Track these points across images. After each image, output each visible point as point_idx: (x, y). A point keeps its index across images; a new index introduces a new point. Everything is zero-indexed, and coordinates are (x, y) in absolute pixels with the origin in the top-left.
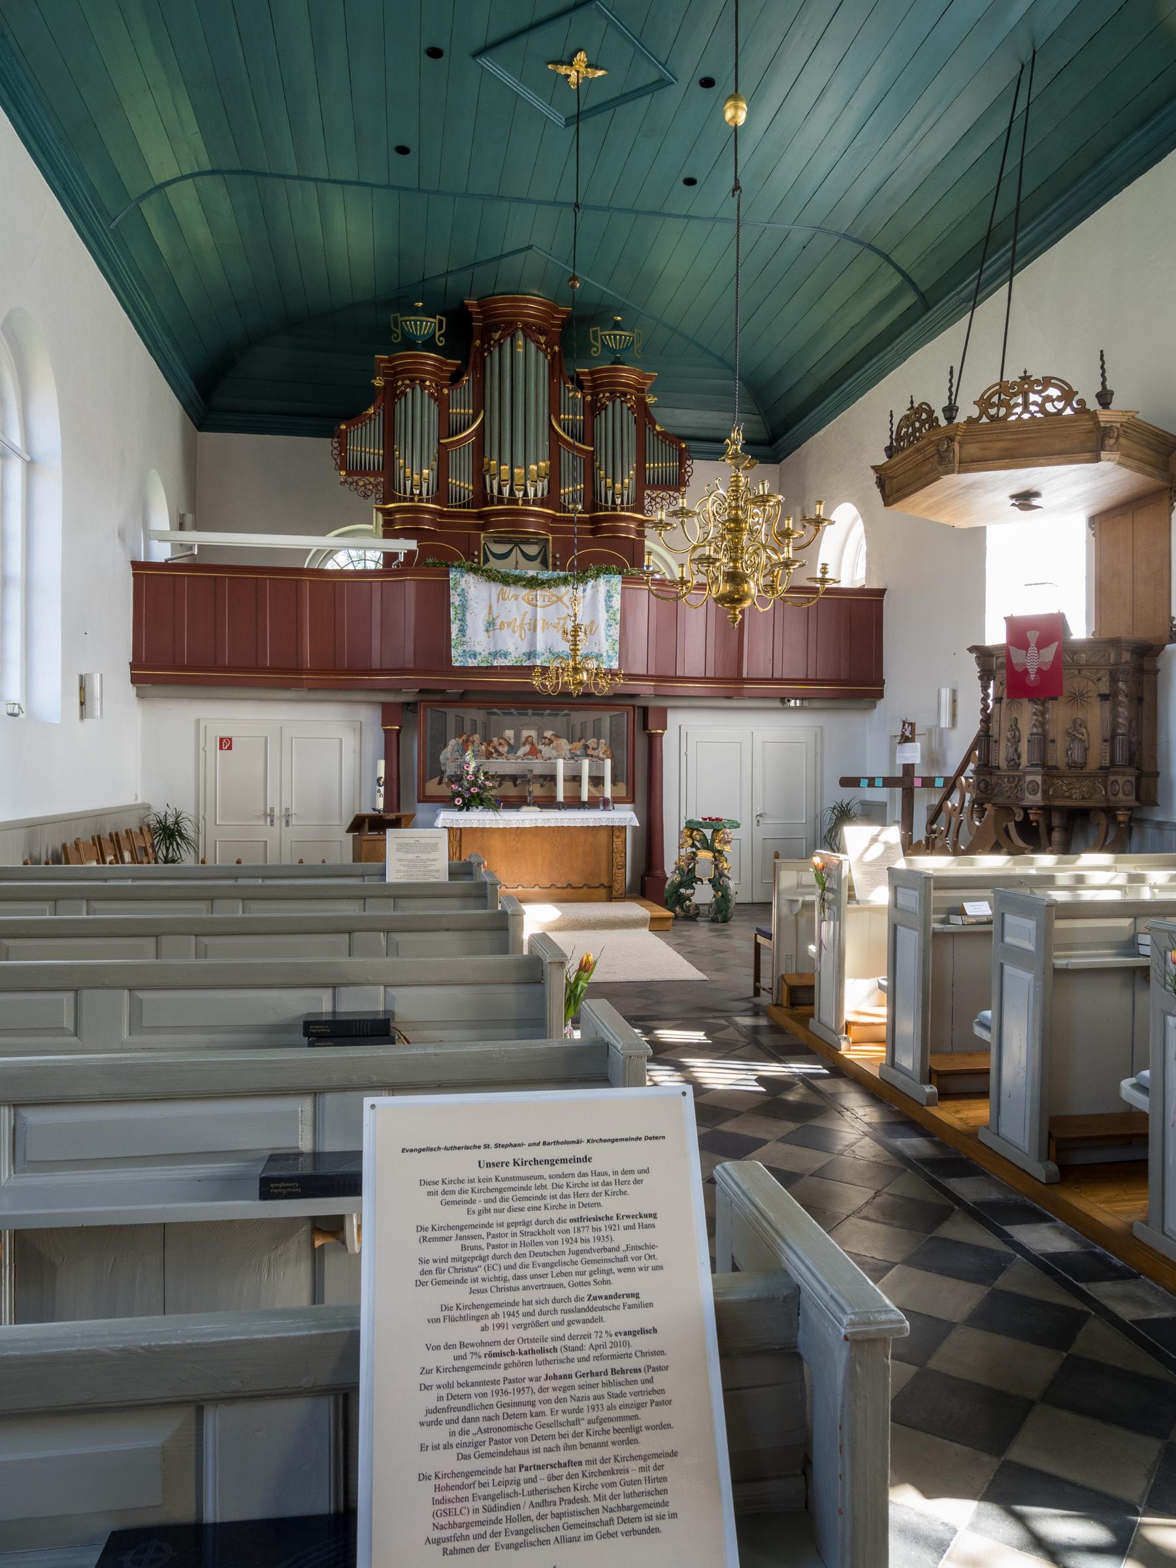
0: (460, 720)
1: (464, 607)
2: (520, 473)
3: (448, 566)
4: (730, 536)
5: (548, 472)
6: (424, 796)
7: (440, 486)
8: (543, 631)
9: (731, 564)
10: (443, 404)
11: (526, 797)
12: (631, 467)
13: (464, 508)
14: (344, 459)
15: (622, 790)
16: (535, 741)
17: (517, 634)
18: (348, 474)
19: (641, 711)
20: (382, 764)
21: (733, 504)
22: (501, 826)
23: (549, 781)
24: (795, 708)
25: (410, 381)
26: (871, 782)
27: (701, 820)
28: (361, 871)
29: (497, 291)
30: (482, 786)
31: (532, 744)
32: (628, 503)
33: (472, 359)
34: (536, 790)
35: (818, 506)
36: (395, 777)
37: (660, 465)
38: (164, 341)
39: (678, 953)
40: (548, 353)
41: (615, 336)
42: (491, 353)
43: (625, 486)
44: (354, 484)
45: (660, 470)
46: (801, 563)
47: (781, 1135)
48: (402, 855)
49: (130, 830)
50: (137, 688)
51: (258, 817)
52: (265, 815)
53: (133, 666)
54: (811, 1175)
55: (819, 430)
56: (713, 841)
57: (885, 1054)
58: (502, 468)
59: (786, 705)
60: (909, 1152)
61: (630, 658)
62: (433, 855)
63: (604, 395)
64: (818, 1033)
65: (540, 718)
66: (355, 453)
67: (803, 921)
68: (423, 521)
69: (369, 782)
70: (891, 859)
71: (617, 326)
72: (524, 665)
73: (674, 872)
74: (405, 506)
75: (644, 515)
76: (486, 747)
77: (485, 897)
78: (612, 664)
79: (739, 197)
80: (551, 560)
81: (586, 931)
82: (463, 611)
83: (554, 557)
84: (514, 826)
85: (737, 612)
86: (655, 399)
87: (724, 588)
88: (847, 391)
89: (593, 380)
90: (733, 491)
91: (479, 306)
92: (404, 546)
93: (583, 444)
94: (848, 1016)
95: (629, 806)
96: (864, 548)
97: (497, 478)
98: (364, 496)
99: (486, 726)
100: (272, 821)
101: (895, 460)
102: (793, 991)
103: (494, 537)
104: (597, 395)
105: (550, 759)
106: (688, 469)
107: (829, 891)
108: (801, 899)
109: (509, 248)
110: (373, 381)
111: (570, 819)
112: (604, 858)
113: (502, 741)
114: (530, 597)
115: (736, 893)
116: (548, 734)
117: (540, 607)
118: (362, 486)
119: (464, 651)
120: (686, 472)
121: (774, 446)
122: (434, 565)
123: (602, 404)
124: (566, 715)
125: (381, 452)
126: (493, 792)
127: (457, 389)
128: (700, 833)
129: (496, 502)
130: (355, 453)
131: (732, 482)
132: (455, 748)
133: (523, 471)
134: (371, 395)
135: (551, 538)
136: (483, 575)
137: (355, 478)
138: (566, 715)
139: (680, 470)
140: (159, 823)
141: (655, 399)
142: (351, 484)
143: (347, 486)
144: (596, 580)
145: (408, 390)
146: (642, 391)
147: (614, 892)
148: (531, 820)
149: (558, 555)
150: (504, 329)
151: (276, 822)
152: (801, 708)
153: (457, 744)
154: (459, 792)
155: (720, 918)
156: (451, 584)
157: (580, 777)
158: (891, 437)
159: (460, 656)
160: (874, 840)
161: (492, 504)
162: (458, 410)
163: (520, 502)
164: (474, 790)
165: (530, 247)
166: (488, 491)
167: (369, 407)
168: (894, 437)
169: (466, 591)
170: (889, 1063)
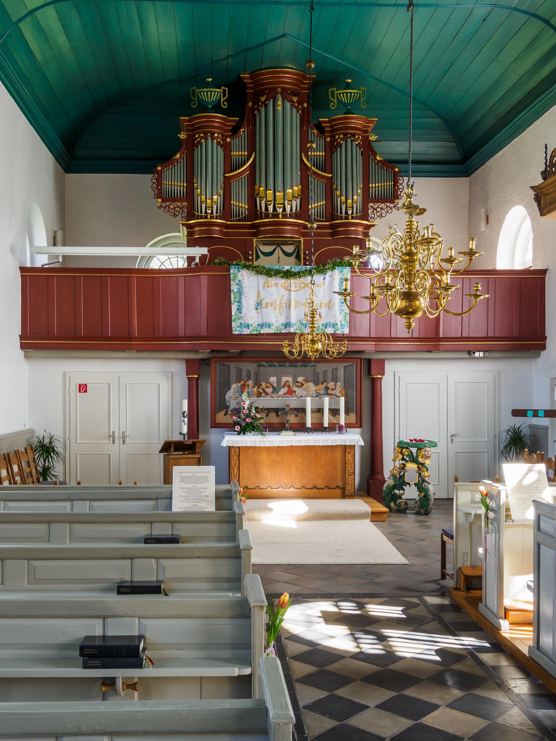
0: (239, 371)
1: (240, 293)
2: (280, 195)
3: (229, 265)
4: (406, 266)
5: (300, 194)
6: (215, 423)
7: (225, 207)
8: (295, 308)
9: (407, 286)
10: (227, 148)
11: (285, 424)
12: (359, 187)
13: (242, 221)
14: (160, 191)
15: (353, 418)
16: (291, 384)
17: (277, 311)
18: (163, 201)
19: (367, 361)
20: (186, 402)
21: (408, 242)
22: (267, 446)
23: (301, 412)
24: (479, 358)
25: (204, 134)
26: (536, 413)
27: (409, 441)
28: (156, 496)
29: (263, 67)
30: (254, 417)
31: (289, 386)
32: (357, 213)
33: (246, 116)
34: (292, 419)
35: (471, 242)
36: (195, 410)
37: (380, 184)
38: (39, 115)
39: (389, 540)
40: (299, 109)
41: (347, 93)
42: (259, 111)
43: (354, 201)
44: (167, 208)
45: (380, 188)
46: (456, 287)
47: (450, 701)
48: (183, 485)
49: (18, 450)
50: (25, 352)
51: (104, 438)
52: (109, 436)
53: (22, 337)
54: (469, 739)
55: (498, 152)
56: (417, 456)
57: (532, 637)
58: (267, 192)
59: (472, 356)
60: (547, 722)
61: (357, 325)
62: (205, 485)
63: (339, 137)
64: (485, 614)
65: (294, 368)
66: (168, 186)
67: (475, 528)
68: (213, 232)
69: (178, 415)
70: (539, 489)
71: (348, 86)
72: (282, 332)
73: (390, 478)
74: (201, 222)
75: (368, 221)
76: (257, 389)
77: (234, 522)
78: (344, 330)
79: (412, 12)
80: (302, 255)
81: (325, 521)
82: (240, 295)
83: (305, 253)
84: (276, 445)
85: (411, 321)
86: (376, 137)
87: (401, 304)
88: (518, 123)
89: (331, 126)
90: (407, 232)
91: (251, 78)
92: (200, 251)
93: (325, 172)
94: (507, 602)
95: (358, 430)
96: (532, 236)
97: (265, 199)
98: (174, 216)
99: (257, 374)
100: (114, 441)
101: (549, 181)
102: (468, 578)
103: (263, 241)
104: (335, 137)
105: (302, 397)
106: (401, 187)
107: (492, 511)
108: (473, 512)
109: (269, 37)
110: (179, 135)
111: (315, 440)
112: (339, 466)
113: (268, 385)
114: (286, 284)
115: (435, 494)
116: (300, 379)
117: (294, 291)
118: (172, 209)
119: (241, 324)
120: (399, 189)
121: (465, 164)
122: (220, 264)
123: (338, 143)
124: (312, 366)
125: (185, 184)
126: (262, 421)
127: (236, 138)
128: (408, 450)
129: (264, 217)
130: (168, 186)
131: (407, 225)
132: (236, 390)
133: (282, 194)
134: (178, 145)
135: (302, 240)
136: (253, 270)
137: (168, 203)
138: (312, 366)
139: (394, 187)
140: (40, 443)
141: (376, 137)
142: (165, 208)
143: (162, 209)
144: (332, 271)
145: (202, 141)
146: (367, 132)
147: (347, 492)
148: (288, 441)
149: (307, 252)
150: (268, 94)
151: (116, 441)
152: (484, 358)
153: (238, 387)
154: (238, 421)
155: (422, 511)
156: (232, 277)
157: (323, 409)
158: (546, 164)
159: (238, 327)
160: (530, 470)
161: (261, 218)
162: (237, 153)
163: (280, 216)
164: (248, 420)
165: (284, 35)
166: (259, 209)
167: (176, 153)
168: (548, 163)
169: (242, 281)
170: (535, 646)
